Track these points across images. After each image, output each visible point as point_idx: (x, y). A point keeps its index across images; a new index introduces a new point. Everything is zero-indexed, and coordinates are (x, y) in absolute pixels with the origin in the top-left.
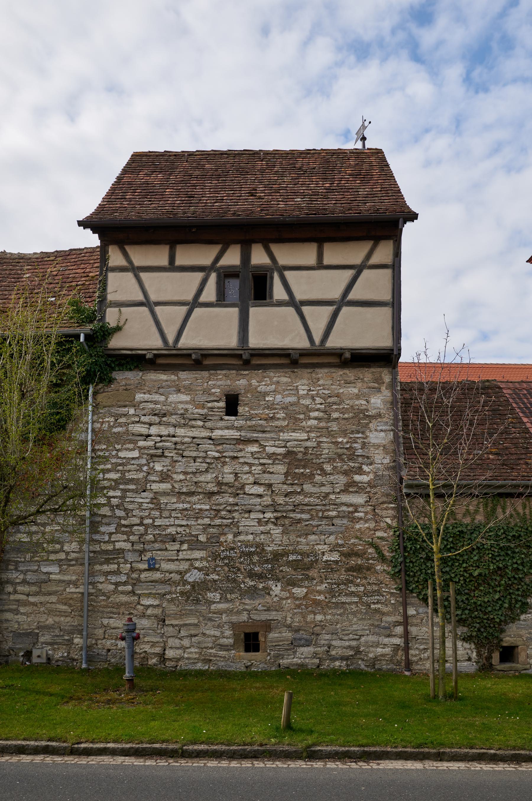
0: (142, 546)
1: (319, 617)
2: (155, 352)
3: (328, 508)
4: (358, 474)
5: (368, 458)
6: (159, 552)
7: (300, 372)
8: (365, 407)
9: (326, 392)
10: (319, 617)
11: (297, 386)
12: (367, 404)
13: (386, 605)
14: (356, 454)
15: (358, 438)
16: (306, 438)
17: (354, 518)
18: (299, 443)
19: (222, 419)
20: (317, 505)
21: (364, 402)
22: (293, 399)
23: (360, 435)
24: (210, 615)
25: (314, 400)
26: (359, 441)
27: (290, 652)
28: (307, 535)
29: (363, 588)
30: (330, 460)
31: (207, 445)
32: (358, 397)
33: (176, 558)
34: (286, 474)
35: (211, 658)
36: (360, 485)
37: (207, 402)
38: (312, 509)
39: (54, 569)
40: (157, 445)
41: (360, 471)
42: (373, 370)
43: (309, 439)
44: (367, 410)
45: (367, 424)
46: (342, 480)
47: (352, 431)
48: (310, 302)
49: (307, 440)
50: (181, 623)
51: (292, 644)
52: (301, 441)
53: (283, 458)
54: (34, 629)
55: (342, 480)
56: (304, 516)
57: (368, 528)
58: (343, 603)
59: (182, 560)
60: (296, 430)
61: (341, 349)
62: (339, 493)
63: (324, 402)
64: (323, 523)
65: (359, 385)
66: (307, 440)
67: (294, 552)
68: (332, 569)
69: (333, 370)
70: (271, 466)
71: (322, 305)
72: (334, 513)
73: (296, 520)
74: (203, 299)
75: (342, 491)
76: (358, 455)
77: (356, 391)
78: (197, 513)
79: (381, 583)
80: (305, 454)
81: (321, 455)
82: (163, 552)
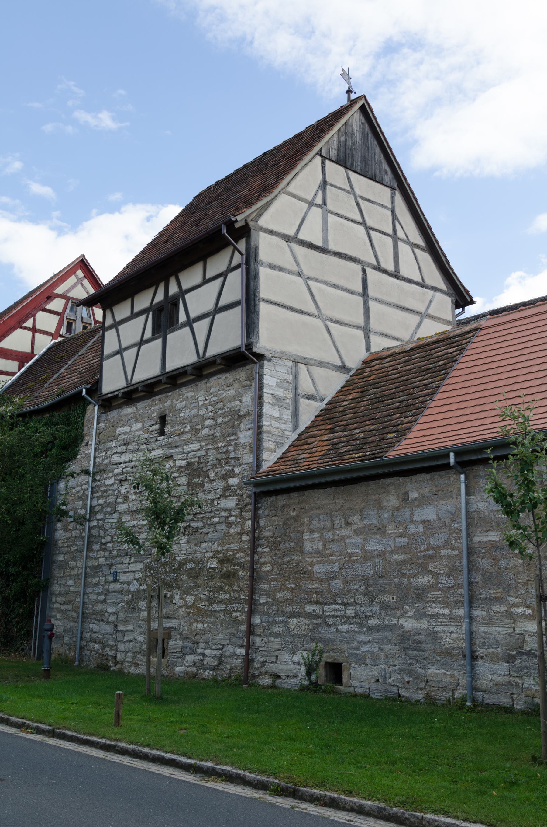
0: (110, 560)
1: (200, 626)
2: (122, 391)
3: (213, 514)
4: (231, 477)
5: (238, 459)
6: (119, 566)
7: (200, 384)
8: (238, 408)
9: (215, 399)
10: (200, 626)
11: (198, 398)
12: (240, 404)
13: (242, 613)
14: (230, 457)
15: (232, 440)
16: (199, 447)
17: (228, 523)
18: (195, 453)
19: (157, 440)
20: (206, 513)
21: (238, 403)
22: (194, 412)
23: (233, 437)
24: (140, 622)
25: (207, 409)
26: (233, 443)
27: (180, 660)
28: (201, 543)
29: (229, 595)
30: (214, 466)
31: (414, 411)
32: (234, 398)
33: (127, 570)
34: (188, 485)
35: (139, 662)
36: (232, 488)
37: (150, 426)
38: (203, 517)
39: (71, 582)
40: (124, 470)
41: (232, 474)
42: (247, 367)
43: (201, 448)
44: (240, 410)
45: (239, 424)
46: (220, 484)
47: (229, 434)
48: (204, 315)
49: (199, 450)
50: (125, 629)
51: (182, 651)
52: (196, 451)
53: (186, 470)
54: (439, 547)
55: (220, 484)
56: (200, 524)
57: (237, 532)
58: (215, 611)
59: (130, 572)
60: (193, 441)
61: (214, 356)
62: (219, 498)
63: (213, 409)
64: (210, 530)
65: (236, 386)
66: (199, 450)
67: (191, 561)
68: (212, 576)
69: (219, 376)
70: (179, 479)
71: (367, 284)
72: (216, 520)
73: (195, 529)
74: (146, 337)
75: (221, 496)
76: (232, 458)
77: (233, 392)
78: (140, 528)
79: (241, 590)
80: (199, 463)
81: (208, 462)
82: (121, 565)
